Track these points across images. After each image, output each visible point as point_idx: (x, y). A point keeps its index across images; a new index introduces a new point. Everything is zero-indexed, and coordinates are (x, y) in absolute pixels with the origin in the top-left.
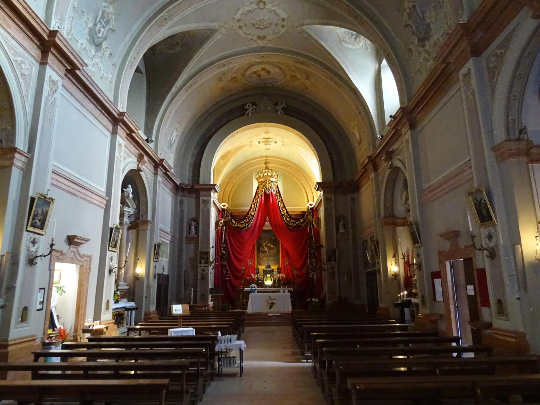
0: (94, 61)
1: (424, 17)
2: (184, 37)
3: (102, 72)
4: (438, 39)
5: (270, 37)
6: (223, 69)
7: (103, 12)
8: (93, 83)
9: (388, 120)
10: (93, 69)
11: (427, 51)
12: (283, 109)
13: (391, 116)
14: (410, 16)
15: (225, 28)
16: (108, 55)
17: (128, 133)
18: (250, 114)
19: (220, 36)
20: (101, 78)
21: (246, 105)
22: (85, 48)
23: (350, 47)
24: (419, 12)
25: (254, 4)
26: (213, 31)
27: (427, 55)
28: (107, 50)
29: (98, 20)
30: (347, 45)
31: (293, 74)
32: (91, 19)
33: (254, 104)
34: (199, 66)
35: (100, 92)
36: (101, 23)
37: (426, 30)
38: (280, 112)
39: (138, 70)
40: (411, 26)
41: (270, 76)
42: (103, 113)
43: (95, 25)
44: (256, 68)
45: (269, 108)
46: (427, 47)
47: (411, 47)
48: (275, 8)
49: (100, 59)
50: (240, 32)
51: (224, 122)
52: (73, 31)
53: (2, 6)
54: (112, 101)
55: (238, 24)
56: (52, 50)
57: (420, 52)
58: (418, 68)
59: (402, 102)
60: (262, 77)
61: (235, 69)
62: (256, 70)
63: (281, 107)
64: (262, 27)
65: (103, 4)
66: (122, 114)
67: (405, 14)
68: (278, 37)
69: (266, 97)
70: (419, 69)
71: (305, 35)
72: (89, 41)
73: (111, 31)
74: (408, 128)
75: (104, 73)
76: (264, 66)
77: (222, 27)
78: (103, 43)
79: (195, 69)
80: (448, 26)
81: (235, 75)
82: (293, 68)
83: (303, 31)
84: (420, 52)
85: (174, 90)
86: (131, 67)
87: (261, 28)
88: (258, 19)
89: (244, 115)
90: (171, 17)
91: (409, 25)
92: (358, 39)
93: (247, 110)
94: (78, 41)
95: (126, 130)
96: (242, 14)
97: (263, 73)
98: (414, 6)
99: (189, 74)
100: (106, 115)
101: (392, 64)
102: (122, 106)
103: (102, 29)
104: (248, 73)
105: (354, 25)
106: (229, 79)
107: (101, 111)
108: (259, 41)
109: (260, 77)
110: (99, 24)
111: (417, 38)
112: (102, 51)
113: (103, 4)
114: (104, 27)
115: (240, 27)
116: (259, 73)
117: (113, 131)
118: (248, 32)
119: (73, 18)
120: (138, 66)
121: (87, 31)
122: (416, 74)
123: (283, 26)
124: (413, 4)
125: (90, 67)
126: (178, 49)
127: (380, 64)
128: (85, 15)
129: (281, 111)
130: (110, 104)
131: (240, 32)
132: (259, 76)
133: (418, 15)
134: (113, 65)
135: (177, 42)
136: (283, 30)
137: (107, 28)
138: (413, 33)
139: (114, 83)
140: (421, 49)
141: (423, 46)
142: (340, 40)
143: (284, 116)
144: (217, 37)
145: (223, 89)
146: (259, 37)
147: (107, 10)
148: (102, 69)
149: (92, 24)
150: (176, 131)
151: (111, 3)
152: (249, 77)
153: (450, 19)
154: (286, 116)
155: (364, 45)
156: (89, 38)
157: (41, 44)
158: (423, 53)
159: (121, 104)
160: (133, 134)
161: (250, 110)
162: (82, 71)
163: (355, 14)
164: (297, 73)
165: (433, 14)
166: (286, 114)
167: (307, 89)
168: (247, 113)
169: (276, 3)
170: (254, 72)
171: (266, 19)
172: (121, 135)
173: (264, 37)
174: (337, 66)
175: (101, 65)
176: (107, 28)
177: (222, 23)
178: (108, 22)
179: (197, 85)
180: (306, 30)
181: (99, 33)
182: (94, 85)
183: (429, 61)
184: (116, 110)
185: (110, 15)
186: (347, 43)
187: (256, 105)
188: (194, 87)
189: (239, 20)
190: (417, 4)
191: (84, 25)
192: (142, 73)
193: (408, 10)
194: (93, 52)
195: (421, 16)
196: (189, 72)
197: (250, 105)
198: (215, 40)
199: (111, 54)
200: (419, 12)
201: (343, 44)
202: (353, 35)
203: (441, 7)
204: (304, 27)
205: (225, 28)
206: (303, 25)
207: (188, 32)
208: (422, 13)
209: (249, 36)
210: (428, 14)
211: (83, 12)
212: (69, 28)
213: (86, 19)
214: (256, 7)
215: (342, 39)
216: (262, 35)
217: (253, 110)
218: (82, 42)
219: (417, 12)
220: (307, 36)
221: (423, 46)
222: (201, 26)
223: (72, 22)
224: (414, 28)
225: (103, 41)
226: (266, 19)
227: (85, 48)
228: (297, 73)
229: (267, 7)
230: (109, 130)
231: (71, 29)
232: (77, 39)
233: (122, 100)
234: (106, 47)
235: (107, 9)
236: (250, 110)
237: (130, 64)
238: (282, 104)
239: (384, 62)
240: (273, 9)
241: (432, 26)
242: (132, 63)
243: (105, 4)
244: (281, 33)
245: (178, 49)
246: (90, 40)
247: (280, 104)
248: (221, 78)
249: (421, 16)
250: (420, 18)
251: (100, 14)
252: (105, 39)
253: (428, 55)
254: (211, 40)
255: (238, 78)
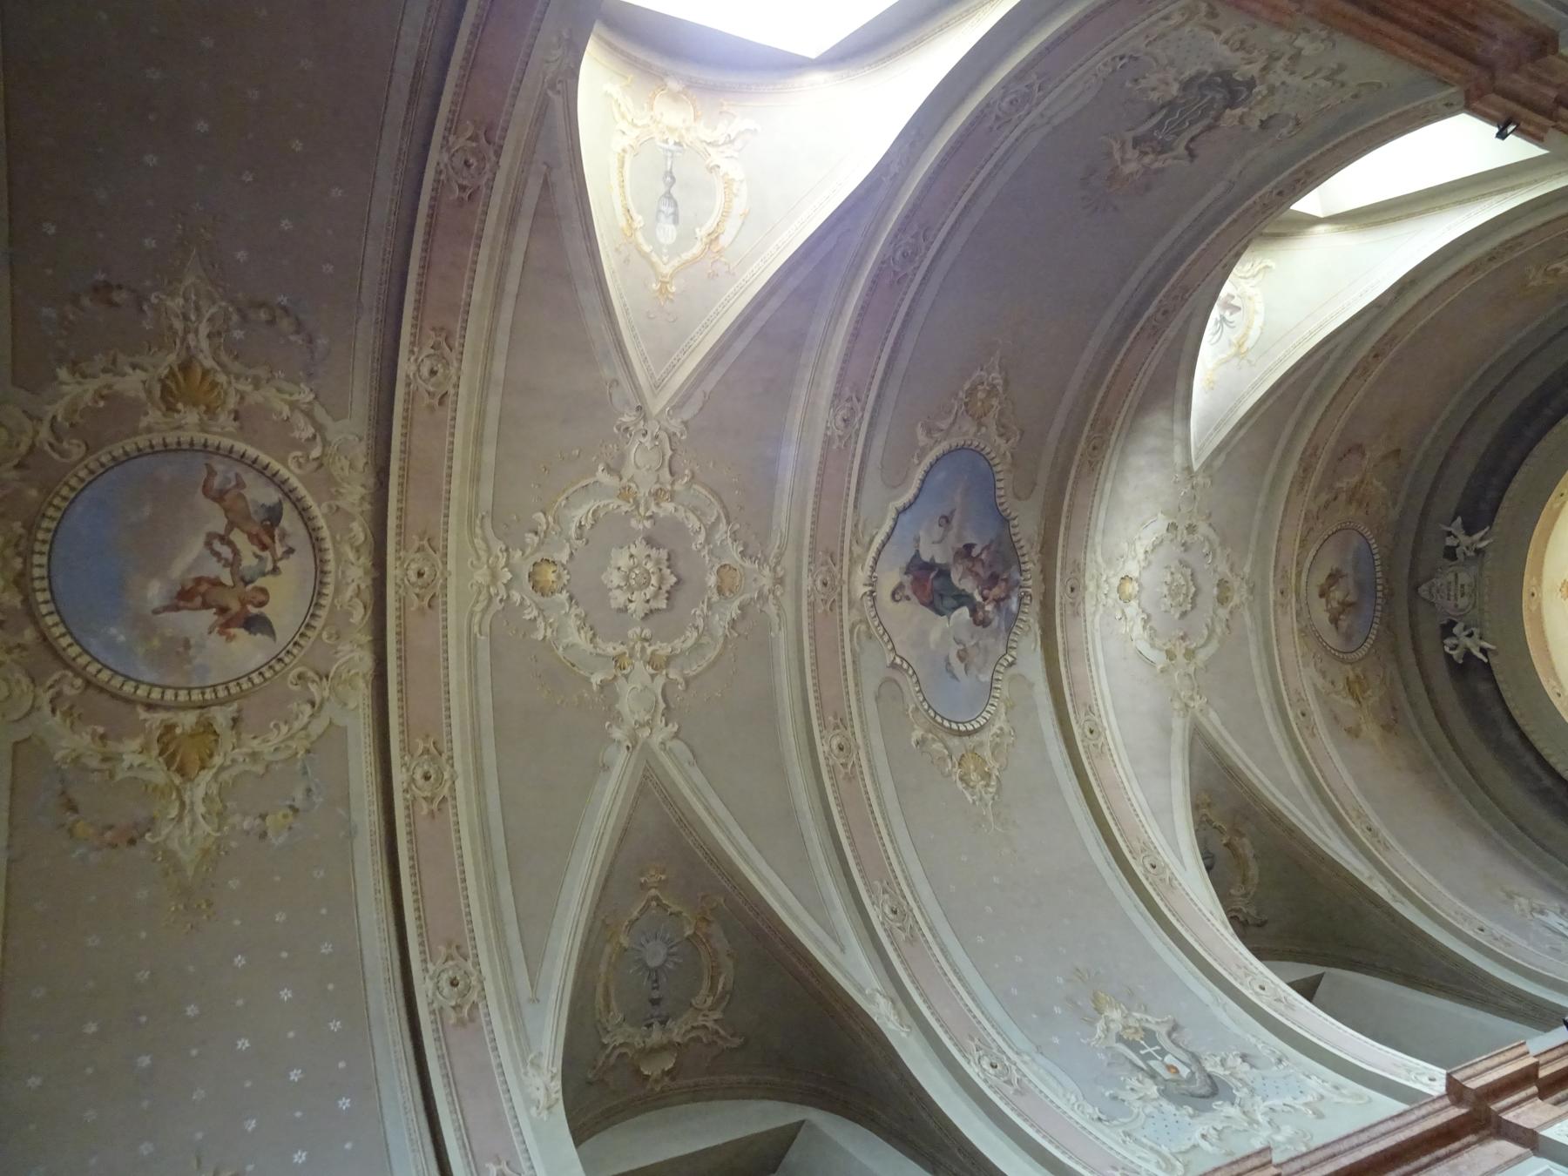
0: (1260, 1118)
1: (1163, 107)
2: (1209, 822)
3: (1298, 1104)
4: (1226, 42)
5: (1223, 568)
6: (1317, 717)
7: (1120, 1039)
8: (1329, 1151)
9: (1518, 149)
10: (1287, 1131)
11: (1265, 69)
12: (1469, 531)
13: (1502, 135)
14: (1164, 148)
15: (1192, 698)
16: (1246, 1067)
17: (1534, 1089)
18: (1486, 645)
19: (1213, 715)
20: (1319, 1115)
21: (1449, 657)
22: (1220, 1132)
23: (1258, 322)
24: (1155, 121)
25: (1127, 611)
26: (1197, 734)
27: (1280, 63)
28: (1230, 1063)
29: (1141, 1063)
30: (1254, 334)
31: (1343, 497)
32: (1134, 1083)
33: (1447, 629)
34: (1306, 796)
35: (1364, 1137)
36: (1149, 1056)
37: (1201, 87)
38: (1482, 539)
39: (1308, 989)
40: (1192, 139)
41: (1348, 570)
42: (1447, 1156)
43: (1153, 1075)
44: (1320, 614)
45: (1464, 578)
46: (1254, 70)
47: (1255, 125)
48: (1141, 551)
49: (1258, 1099)
50: (1202, 656)
51: (1511, 737)
52: (1164, 1150)
53: (1406, 1169)
54: (1402, 1107)
55: (1180, 658)
56: (1496, 1107)
57: (1272, 90)
58: (1323, 83)
59: (1448, 110)
60: (1350, 599)
61: (1320, 682)
62: (1325, 617)
63: (1464, 539)
64: (1193, 590)
65: (1099, 1033)
66: (1455, 1090)
67: (1157, 165)
68: (1223, 544)
69: (1424, 587)
70: (1327, 78)
71: (1219, 462)
72: (1199, 1111)
73: (1174, 1035)
74: (1550, 57)
75: (1303, 1099)
76: (1315, 592)
77: (1187, 706)
78: (1209, 1069)
79: (1314, 809)
80: (1188, 20)
81: (1341, 684)
82: (1324, 497)
83: (1207, 465)
84: (1272, 90)
85: (1381, 888)
86: (1290, 1006)
87: (1195, 594)
88: (1168, 601)
89: (1488, 666)
90: (1147, 848)
91: (1187, 148)
92: (1236, 302)
93: (1468, 655)
94: (1195, 1146)
95: (1523, 1094)
96: (1153, 646)
97: (1337, 594)
98: (1136, 142)
99: (1328, 830)
100: (1456, 1145)
101: (1309, 173)
102: (1425, 1079)
103: (1169, 1059)
104: (1332, 639)
105: (1190, 316)
106: (1353, 704)
107: (1439, 1160)
108: (1236, 600)
109: (1351, 604)
110: (1152, 1063)
111: (1228, 111)
112: (1233, 1082)
113: (1099, 1033)
114: (1163, 1053)
115: (1190, 654)
116: (1335, 604)
117: (1523, 1145)
118: (1206, 632)
119: (1127, 1134)
120: (1291, 985)
121: (1169, 1108)
122: (1343, 85)
123: (1191, 529)
124: (1129, 144)
125: (1279, 1138)
126: (1246, 847)
127: (1314, 221)
128: (1122, 1095)
129: (1477, 536)
130: (1413, 1117)
131: (1202, 656)
132: (1346, 606)
133: (1159, 126)
134: (1280, 1061)
135: (1226, 845)
136: (1203, 528)
137: (1166, 1043)
138: (1209, 128)
139: (1342, 1080)
140: (1261, 89)
141: (1251, 84)
142: (1237, 355)
143: (1496, 529)
144: (1213, 722)
145: (1387, 728)
146: (1222, 600)
147: (1116, 1027)
148: (1289, 1100)
149: (1148, 1082)
150: (1542, 912)
151: (1099, 1011)
152: (1348, 637)
153: (1166, 18)
154: (1497, 520)
155: (1254, 282)
156: (1190, 1110)
157: (1475, 1132)
158: (1272, 78)
159: (1416, 1080)
160: (1543, 1073)
161: (1468, 642)
162: (1542, 1060)
163: (1159, 316)
164: (1339, 485)
165: (1153, 79)
166: (1491, 523)
167: (1398, 452)
168: (1480, 656)
169: (1125, 546)
170: (1335, 621)
171: (1169, 579)
172: (1545, 1119)
173: (1223, 584)
174: (1317, 357)
175: (1276, 1102)
176: (1166, 1043)
177: (1177, 705)
178: (1150, 1036)
179: (1367, 809)
180: (1203, 459)
181: (1177, 1071)
182: (1336, 1149)
183: (1300, 50)
184: (1437, 1106)
185: (1131, 1022)
186: (1245, 335)
187: (1453, 624)
188: (1375, 822)
189: (1170, 655)
190: (1129, 136)
191: (1149, 1109)
192: (1321, 976)
193: (1147, 160)
194: (1233, 1111)
195: (1164, 111)
196: (1321, 829)
197: (1447, 641)
198: (1225, 734)
199: (1244, 1057)
200: (1155, 121)
201: (1249, 344)
202: (1223, 319)
203: (1136, 59)
204: (1196, 467)
205: (1192, 698)
206: (1189, 469)
207: (1196, 807)
208: (1153, 114)
209: (1218, 630)
210: (1154, 96)
211: (1114, 1098)
212: (1154, 1158)
213: (1136, 1096)
214: (1134, 603)
215: (1233, 350)
216: (1215, 591)
217: (1470, 635)
218: (1197, 1135)
219: (1152, 130)
220: (1222, 457)
221: (1251, 84)
222: (1180, 769)
223: (1136, 1141)
224: (1196, 129)
225: (1203, 1070)
226: (1169, 579)
227: (1220, 1132)
228: (1339, 485)
229: (1135, 574)
230: (1519, 1159)
231: (1158, 1153)
232: (1189, 1145)
233: (1404, 1073)
234: (1223, 1063)
235: (1112, 1026)
236: (1468, 642)
237: (1281, 1007)
238: (1450, 534)
239: (1307, 205)
240: (1141, 556)
241: (1188, 73)
242: (1279, 1000)
243: (1100, 1025)
244: (1213, 536)
245: (1246, 847)
246: (1195, 1109)
247: (1450, 542)
248: (1349, 731)
249: (1164, 111)
250: (1166, 117)
251: (1122, 1048)
252: (1196, 1058)
253: (1278, 59)
254: (1221, 743)
255: (1351, 676)
